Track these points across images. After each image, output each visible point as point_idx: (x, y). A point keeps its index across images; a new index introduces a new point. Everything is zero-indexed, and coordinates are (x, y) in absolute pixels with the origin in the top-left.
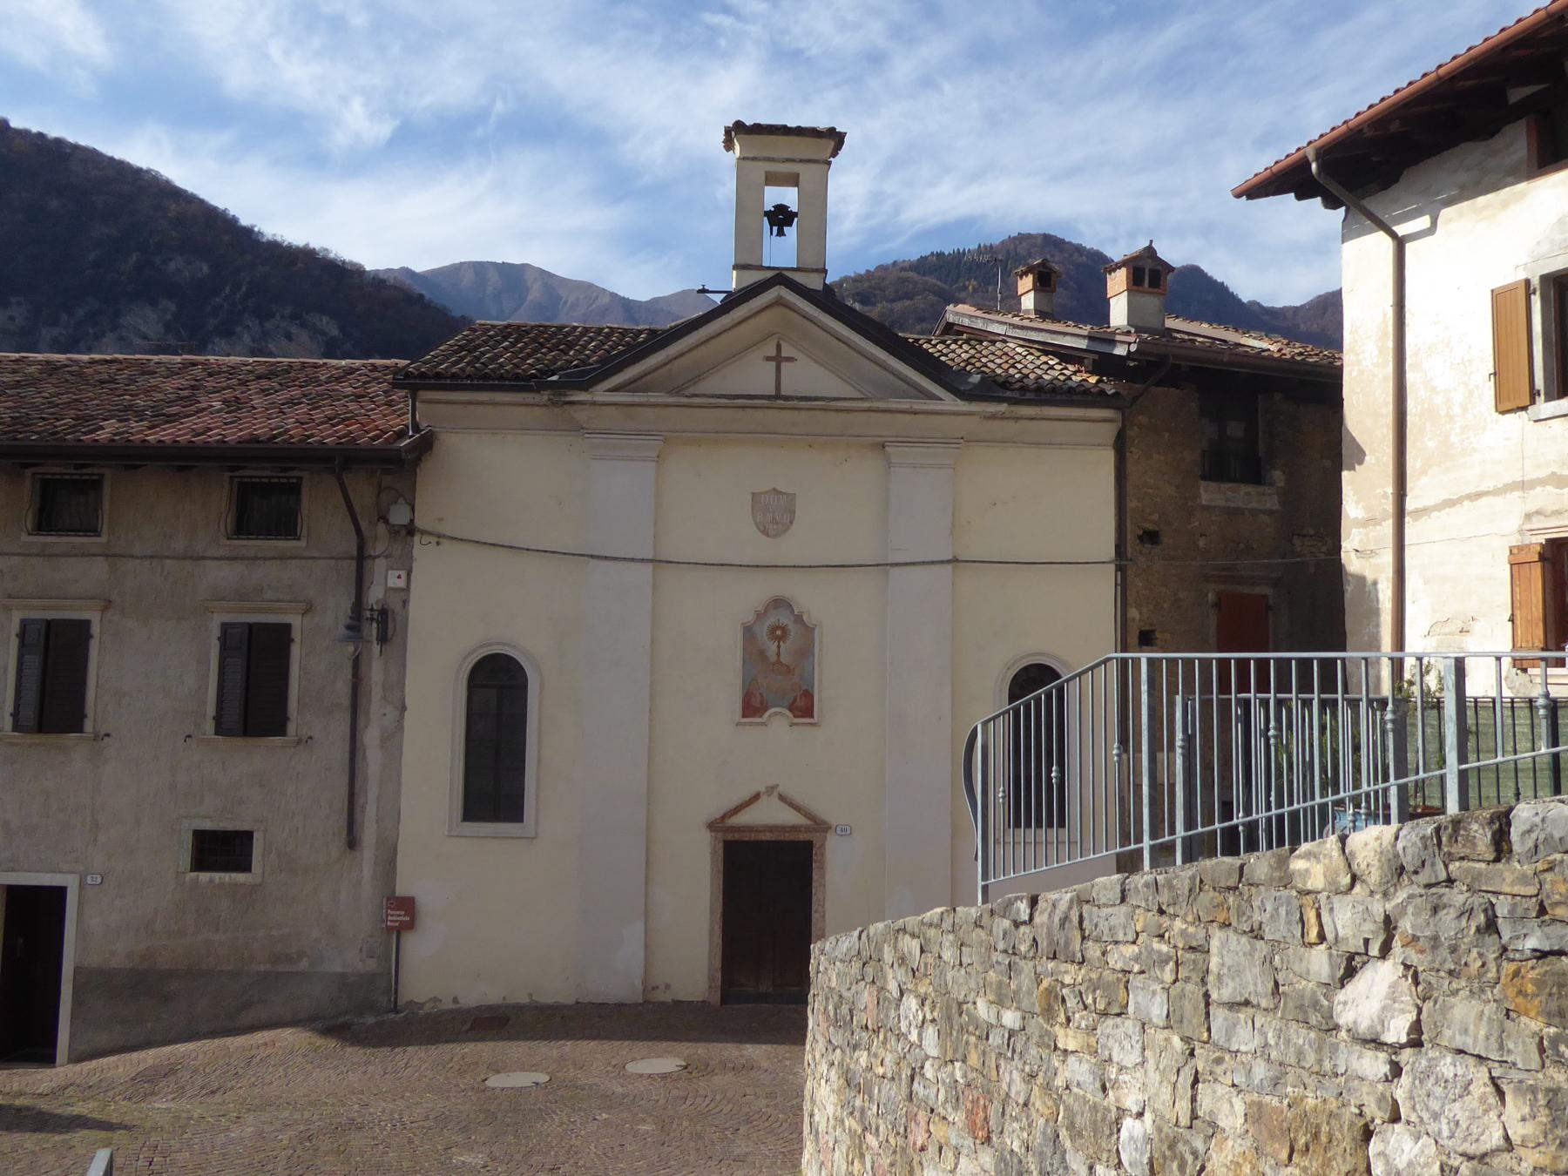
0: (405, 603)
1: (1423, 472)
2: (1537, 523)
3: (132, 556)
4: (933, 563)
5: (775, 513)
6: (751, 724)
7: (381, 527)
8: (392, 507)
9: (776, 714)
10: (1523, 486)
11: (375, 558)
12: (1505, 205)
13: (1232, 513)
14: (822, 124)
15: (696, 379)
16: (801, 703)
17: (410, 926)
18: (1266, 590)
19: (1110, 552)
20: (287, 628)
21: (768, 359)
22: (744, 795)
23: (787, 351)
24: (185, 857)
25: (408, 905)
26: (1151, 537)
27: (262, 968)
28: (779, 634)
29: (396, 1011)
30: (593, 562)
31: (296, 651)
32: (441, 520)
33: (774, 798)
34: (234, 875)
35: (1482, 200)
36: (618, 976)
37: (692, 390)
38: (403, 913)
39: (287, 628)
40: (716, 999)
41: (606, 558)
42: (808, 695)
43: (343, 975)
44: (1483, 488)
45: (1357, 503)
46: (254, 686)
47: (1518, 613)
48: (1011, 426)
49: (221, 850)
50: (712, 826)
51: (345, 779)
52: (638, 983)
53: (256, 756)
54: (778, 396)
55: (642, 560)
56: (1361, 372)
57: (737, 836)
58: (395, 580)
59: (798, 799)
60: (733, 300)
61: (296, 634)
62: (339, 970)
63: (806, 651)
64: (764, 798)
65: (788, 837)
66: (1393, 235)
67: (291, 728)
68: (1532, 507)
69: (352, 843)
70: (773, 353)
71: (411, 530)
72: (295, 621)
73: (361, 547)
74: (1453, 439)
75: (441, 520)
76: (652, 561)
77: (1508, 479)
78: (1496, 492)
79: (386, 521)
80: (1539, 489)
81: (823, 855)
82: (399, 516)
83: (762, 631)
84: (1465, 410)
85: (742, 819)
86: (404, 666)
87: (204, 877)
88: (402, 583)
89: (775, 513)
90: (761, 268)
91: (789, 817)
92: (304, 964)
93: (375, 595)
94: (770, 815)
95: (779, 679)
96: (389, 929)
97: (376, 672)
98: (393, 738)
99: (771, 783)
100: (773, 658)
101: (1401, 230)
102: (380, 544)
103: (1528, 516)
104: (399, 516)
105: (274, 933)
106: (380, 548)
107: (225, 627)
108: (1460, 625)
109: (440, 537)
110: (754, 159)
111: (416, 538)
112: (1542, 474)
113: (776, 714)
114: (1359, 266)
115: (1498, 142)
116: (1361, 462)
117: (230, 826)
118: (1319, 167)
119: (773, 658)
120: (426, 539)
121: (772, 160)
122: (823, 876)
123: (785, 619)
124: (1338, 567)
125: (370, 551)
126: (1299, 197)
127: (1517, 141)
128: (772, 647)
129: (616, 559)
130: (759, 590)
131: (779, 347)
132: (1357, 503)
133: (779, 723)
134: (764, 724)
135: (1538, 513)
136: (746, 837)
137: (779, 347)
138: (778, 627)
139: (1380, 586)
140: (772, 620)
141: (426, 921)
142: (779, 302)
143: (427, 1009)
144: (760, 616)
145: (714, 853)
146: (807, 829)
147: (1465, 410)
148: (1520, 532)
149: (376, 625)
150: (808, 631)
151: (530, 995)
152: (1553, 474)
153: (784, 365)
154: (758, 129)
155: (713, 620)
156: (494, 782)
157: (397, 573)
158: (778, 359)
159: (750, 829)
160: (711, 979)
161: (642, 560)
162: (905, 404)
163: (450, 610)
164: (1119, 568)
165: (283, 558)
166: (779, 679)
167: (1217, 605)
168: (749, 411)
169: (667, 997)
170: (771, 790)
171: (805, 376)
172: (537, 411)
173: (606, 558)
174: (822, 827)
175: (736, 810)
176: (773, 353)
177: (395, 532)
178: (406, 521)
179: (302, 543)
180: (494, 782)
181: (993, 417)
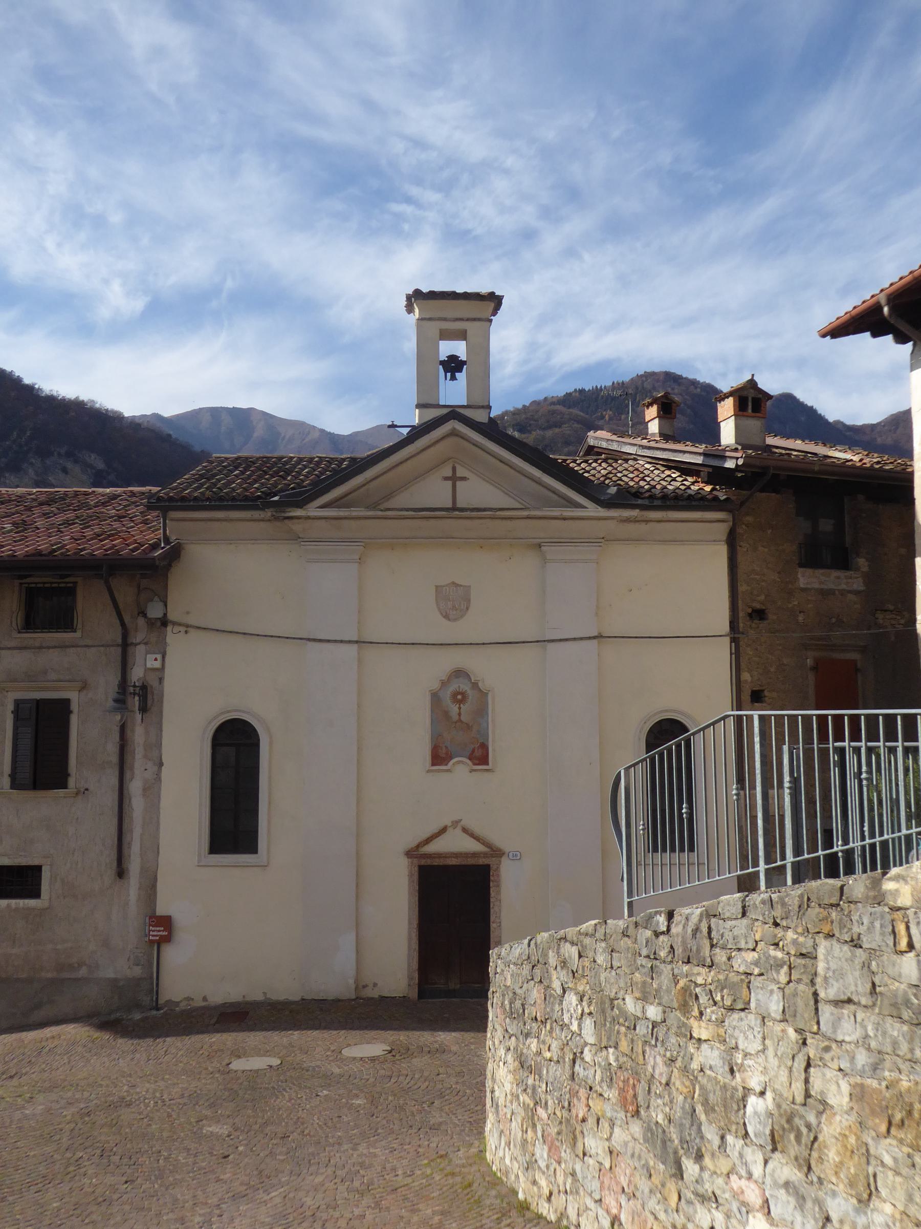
0: (161, 680)
4: (581, 639)
5: (454, 601)
6: (439, 771)
7: (141, 621)
13: (825, 593)
15: (389, 496)
16: (478, 753)
17: (168, 939)
20: (67, 701)
21: (446, 479)
23: (461, 472)
25: (166, 922)
27: (50, 975)
28: (459, 698)
31: (74, 720)
32: (188, 613)
33: (458, 831)
34: (26, 901)
36: (334, 978)
37: (382, 507)
39: (67, 701)
40: (414, 994)
41: (320, 641)
42: (484, 747)
43: (115, 980)
50: (409, 854)
52: (351, 981)
53: (44, 805)
55: (350, 642)
57: (429, 862)
58: (152, 662)
59: (477, 830)
61: (74, 707)
62: (111, 975)
63: (482, 711)
65: (471, 861)
67: (71, 782)
69: (121, 873)
70: (450, 474)
71: (164, 622)
72: (73, 696)
73: (125, 635)
76: (357, 642)
81: (498, 876)
82: (155, 611)
83: (446, 696)
85: (432, 848)
86: (161, 731)
88: (157, 664)
89: (454, 601)
90: (438, 406)
91: (471, 846)
92: (83, 972)
94: (455, 844)
95: (460, 735)
97: (138, 735)
98: (153, 789)
99: (456, 818)
100: (455, 717)
104: (155, 611)
105: (59, 947)
106: (139, 637)
107: (18, 703)
110: (430, 319)
111: (169, 628)
118: (890, 310)
119: (455, 717)
121: (445, 319)
122: (499, 893)
123: (465, 687)
125: (131, 640)
128: (454, 709)
129: (329, 641)
131: (454, 469)
133: (460, 771)
136: (436, 862)
137: (454, 469)
138: (459, 693)
140: (453, 687)
142: (454, 433)
143: (183, 1006)
144: (444, 684)
145: (411, 875)
146: (485, 855)
149: (139, 699)
150: (483, 695)
151: (265, 993)
153: (458, 483)
155: (405, 693)
156: (233, 825)
157: (155, 656)
158: (454, 479)
159: (439, 855)
160: (410, 978)
161: (350, 642)
162: (556, 512)
163: (197, 685)
164: (734, 640)
165: (63, 647)
166: (460, 735)
167: (815, 668)
169: (375, 994)
170: (455, 823)
173: (320, 641)
174: (498, 853)
175: (428, 841)
176: (450, 474)
177: (151, 623)
178: (160, 615)
179: (78, 634)
180: (233, 825)
181: (628, 520)
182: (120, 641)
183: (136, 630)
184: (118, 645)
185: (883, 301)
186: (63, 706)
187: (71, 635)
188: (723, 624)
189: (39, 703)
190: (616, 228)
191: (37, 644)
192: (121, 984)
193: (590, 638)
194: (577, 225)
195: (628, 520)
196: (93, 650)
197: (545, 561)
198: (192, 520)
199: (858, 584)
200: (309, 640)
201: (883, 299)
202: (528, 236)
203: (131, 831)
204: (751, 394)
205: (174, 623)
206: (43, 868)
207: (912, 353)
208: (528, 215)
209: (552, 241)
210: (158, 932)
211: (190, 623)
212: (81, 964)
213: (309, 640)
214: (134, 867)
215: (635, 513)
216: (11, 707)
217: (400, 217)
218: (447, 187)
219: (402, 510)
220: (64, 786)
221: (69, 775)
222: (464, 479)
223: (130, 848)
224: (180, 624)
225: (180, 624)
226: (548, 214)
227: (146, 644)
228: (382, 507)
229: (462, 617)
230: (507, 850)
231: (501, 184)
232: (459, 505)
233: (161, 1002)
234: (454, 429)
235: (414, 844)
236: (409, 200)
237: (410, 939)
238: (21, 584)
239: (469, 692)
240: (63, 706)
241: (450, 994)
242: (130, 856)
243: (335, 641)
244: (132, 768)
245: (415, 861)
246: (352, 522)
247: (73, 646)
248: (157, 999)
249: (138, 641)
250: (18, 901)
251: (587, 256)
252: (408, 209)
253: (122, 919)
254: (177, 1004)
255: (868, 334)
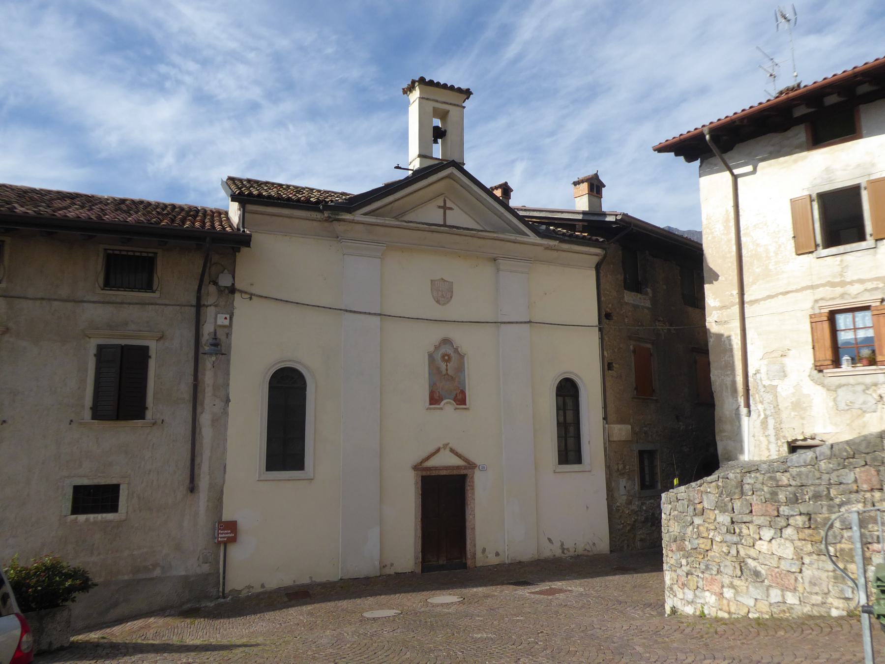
0: (228, 335)
1: (754, 283)
2: (821, 304)
3: (27, 298)
4: (521, 323)
5: (443, 292)
6: (434, 409)
7: (212, 288)
8: (221, 275)
9: (447, 403)
10: (812, 287)
11: (207, 306)
12: (795, 161)
13: (636, 307)
14: (464, 87)
15: (403, 213)
16: (459, 397)
17: (234, 540)
18: (649, 346)
19: (596, 322)
20: (146, 349)
21: (439, 207)
22: (431, 449)
23: (449, 204)
24: (68, 505)
25: (232, 526)
26: (608, 316)
27: (126, 577)
28: (446, 358)
29: (224, 596)
30: (347, 314)
31: (152, 364)
32: (252, 285)
33: (447, 451)
34: (104, 515)
35: (782, 159)
36: (364, 563)
37: (407, 218)
38: (228, 532)
39: (146, 349)
40: (419, 570)
41: (355, 312)
42: (463, 393)
43: (186, 578)
44: (789, 289)
45: (715, 299)
46: (122, 387)
47: (816, 345)
48: (555, 254)
49: (95, 498)
50: (416, 468)
51: (189, 446)
52: (377, 563)
53: (124, 434)
54: (445, 225)
55: (375, 314)
56: (714, 238)
57: (428, 473)
58: (222, 320)
59: (460, 451)
60: (419, 175)
61: (152, 353)
62: (183, 573)
63: (460, 369)
64: (442, 451)
65: (455, 472)
66: (732, 174)
67: (149, 414)
68: (818, 297)
69: (192, 488)
70: (442, 204)
71: (232, 290)
72: (153, 345)
73: (199, 299)
74: (771, 267)
75: (252, 285)
76: (380, 315)
77: (805, 285)
78: (797, 291)
79: (215, 283)
80: (821, 289)
81: (473, 482)
82: (225, 281)
83: (438, 357)
84: (777, 254)
85: (430, 463)
86: (228, 374)
87: (82, 518)
88: (227, 322)
89: (443, 292)
90: (432, 158)
91: (455, 461)
92: (157, 572)
93: (208, 329)
94: (445, 460)
95: (447, 385)
96: (219, 543)
97: (208, 378)
98: (220, 421)
99: (445, 442)
100: (444, 372)
101: (736, 171)
102: (211, 296)
103: (816, 301)
104: (225, 281)
105: (135, 552)
106: (211, 300)
107: (101, 348)
108: (781, 353)
109: (251, 296)
110: (427, 99)
111: (237, 296)
112: (823, 281)
113: (447, 403)
114: (714, 186)
115: (789, 133)
116: (717, 279)
117: (103, 481)
118: (711, 137)
119: (444, 372)
120: (244, 296)
121: (437, 101)
122: (473, 494)
123: (450, 351)
124: (704, 330)
125: (204, 302)
126: (676, 155)
127: (801, 134)
128: (443, 366)
129: (360, 313)
130: (437, 333)
131: (445, 202)
132: (715, 299)
133: (448, 408)
134: (441, 409)
135: (822, 299)
136: (434, 473)
137: (445, 202)
138: (446, 355)
139: (733, 338)
140: (443, 350)
141: (243, 537)
142: (448, 177)
143: (243, 594)
144: (437, 348)
145: (416, 483)
146: (465, 468)
147: (777, 254)
148: (813, 308)
149: (210, 350)
150: (461, 357)
151: (311, 578)
152: (829, 282)
153: (447, 211)
154: (431, 83)
155: (413, 350)
156: (286, 446)
157: (224, 316)
158: (445, 208)
159: (436, 468)
160: (416, 558)
161: (375, 314)
162: (513, 237)
163: (257, 341)
164: (600, 330)
165: (143, 304)
166: (447, 385)
167: (634, 351)
168: (435, 234)
169: (392, 572)
170: (445, 446)
171: (457, 217)
172: (315, 224)
173: (355, 312)
174: (472, 466)
175: (428, 458)
176: (442, 204)
177: (221, 290)
178: (229, 284)
179: (157, 295)
180: (286, 446)
181: (548, 248)
182: (194, 302)
183: (208, 294)
184: (192, 306)
185: (706, 130)
186: (143, 352)
187: (152, 295)
188: (595, 321)
189: (123, 348)
190: (314, 114)
191: (119, 300)
192: (192, 579)
193: (525, 322)
194: (288, 106)
195: (548, 248)
196: (171, 308)
197: (498, 270)
198: (262, 214)
199: (648, 304)
200: (346, 311)
201: (706, 130)
202: (254, 107)
203: (202, 455)
204: (595, 183)
205: (241, 292)
206: (121, 487)
207: (700, 166)
208: (255, 93)
209: (270, 113)
210: (224, 535)
211: (254, 292)
212: (155, 566)
213: (346, 311)
214: (203, 483)
215: (556, 243)
216: (93, 351)
217: (165, 77)
218: (205, 63)
219: (419, 223)
220: (143, 417)
221: (147, 408)
222: (451, 209)
223: (199, 468)
224: (246, 293)
225: (246, 293)
226: (272, 97)
227: (216, 306)
228: (407, 218)
229: (448, 302)
230: (478, 463)
231: (242, 69)
232: (448, 223)
233: (227, 591)
234: (452, 173)
235: (419, 460)
236: (174, 66)
237: (416, 530)
238: (105, 250)
239: (452, 354)
240: (143, 352)
241: (441, 568)
242: (200, 475)
243: (365, 313)
244: (202, 404)
245: (420, 473)
246: (382, 229)
247: (152, 304)
248: (224, 589)
249: (209, 303)
250: (96, 515)
251: (291, 127)
252: (173, 72)
253: (192, 528)
254: (240, 592)
255: (673, 154)
